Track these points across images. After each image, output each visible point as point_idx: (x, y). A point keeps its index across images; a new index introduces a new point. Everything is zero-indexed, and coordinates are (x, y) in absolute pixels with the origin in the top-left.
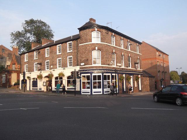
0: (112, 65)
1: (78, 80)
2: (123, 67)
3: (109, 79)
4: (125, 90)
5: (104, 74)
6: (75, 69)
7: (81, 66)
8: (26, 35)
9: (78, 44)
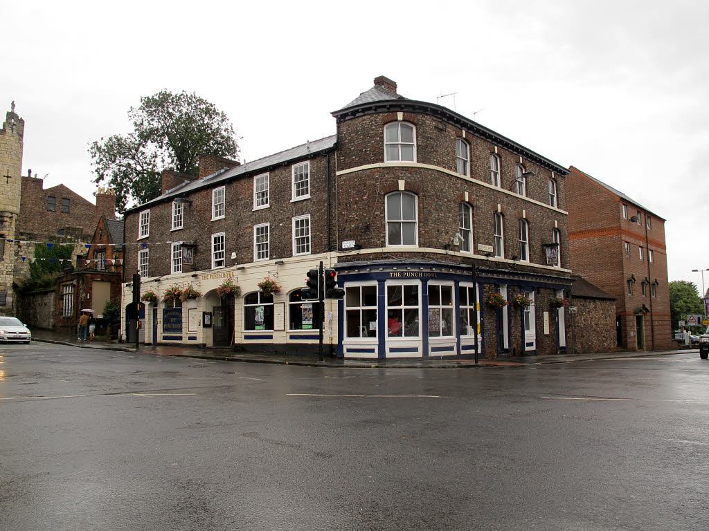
0: (458, 248)
2: (500, 258)
3: (447, 300)
4: (506, 346)
5: (430, 283)
6: (321, 263)
7: (341, 250)
8: (141, 148)
9: (330, 170)
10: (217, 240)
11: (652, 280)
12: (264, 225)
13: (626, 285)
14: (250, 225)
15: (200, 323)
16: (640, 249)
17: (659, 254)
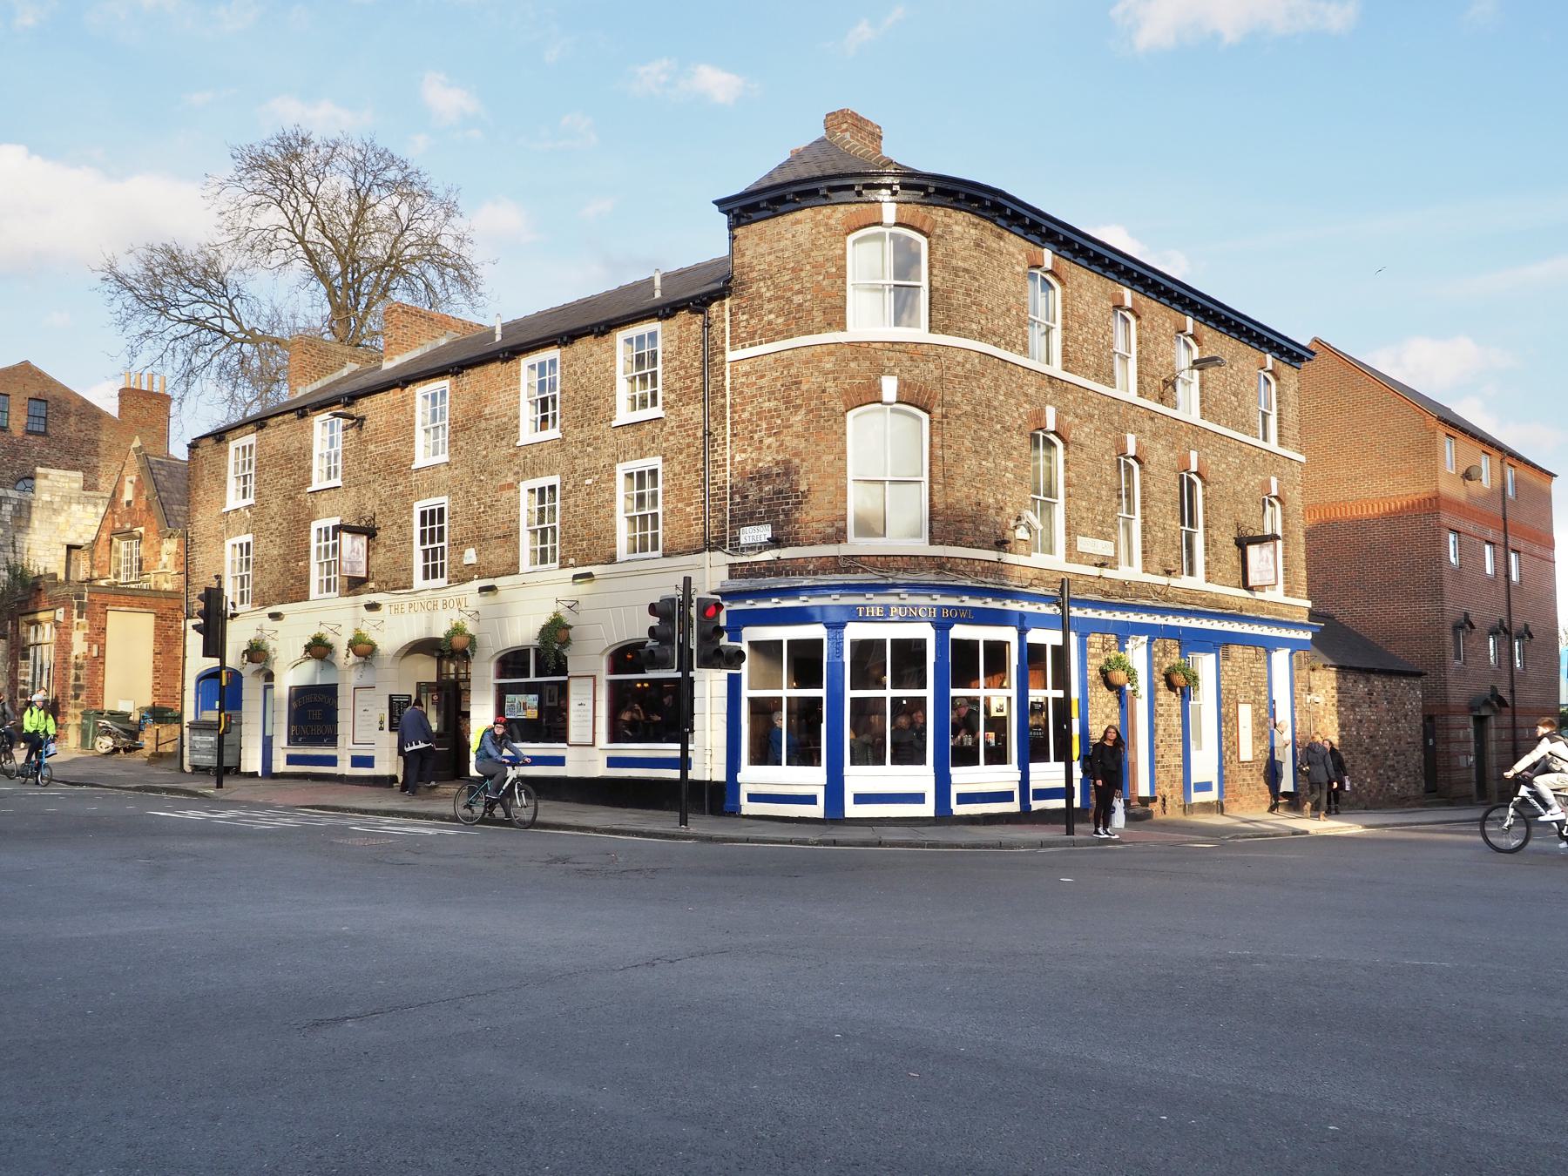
1: (710, 686)
5: (959, 632)
6: (687, 581)
7: (736, 548)
10: (430, 517)
11: (1518, 623)
12: (545, 481)
13: (1449, 639)
14: (510, 480)
15: (381, 722)
16: (1487, 547)
17: (1537, 560)
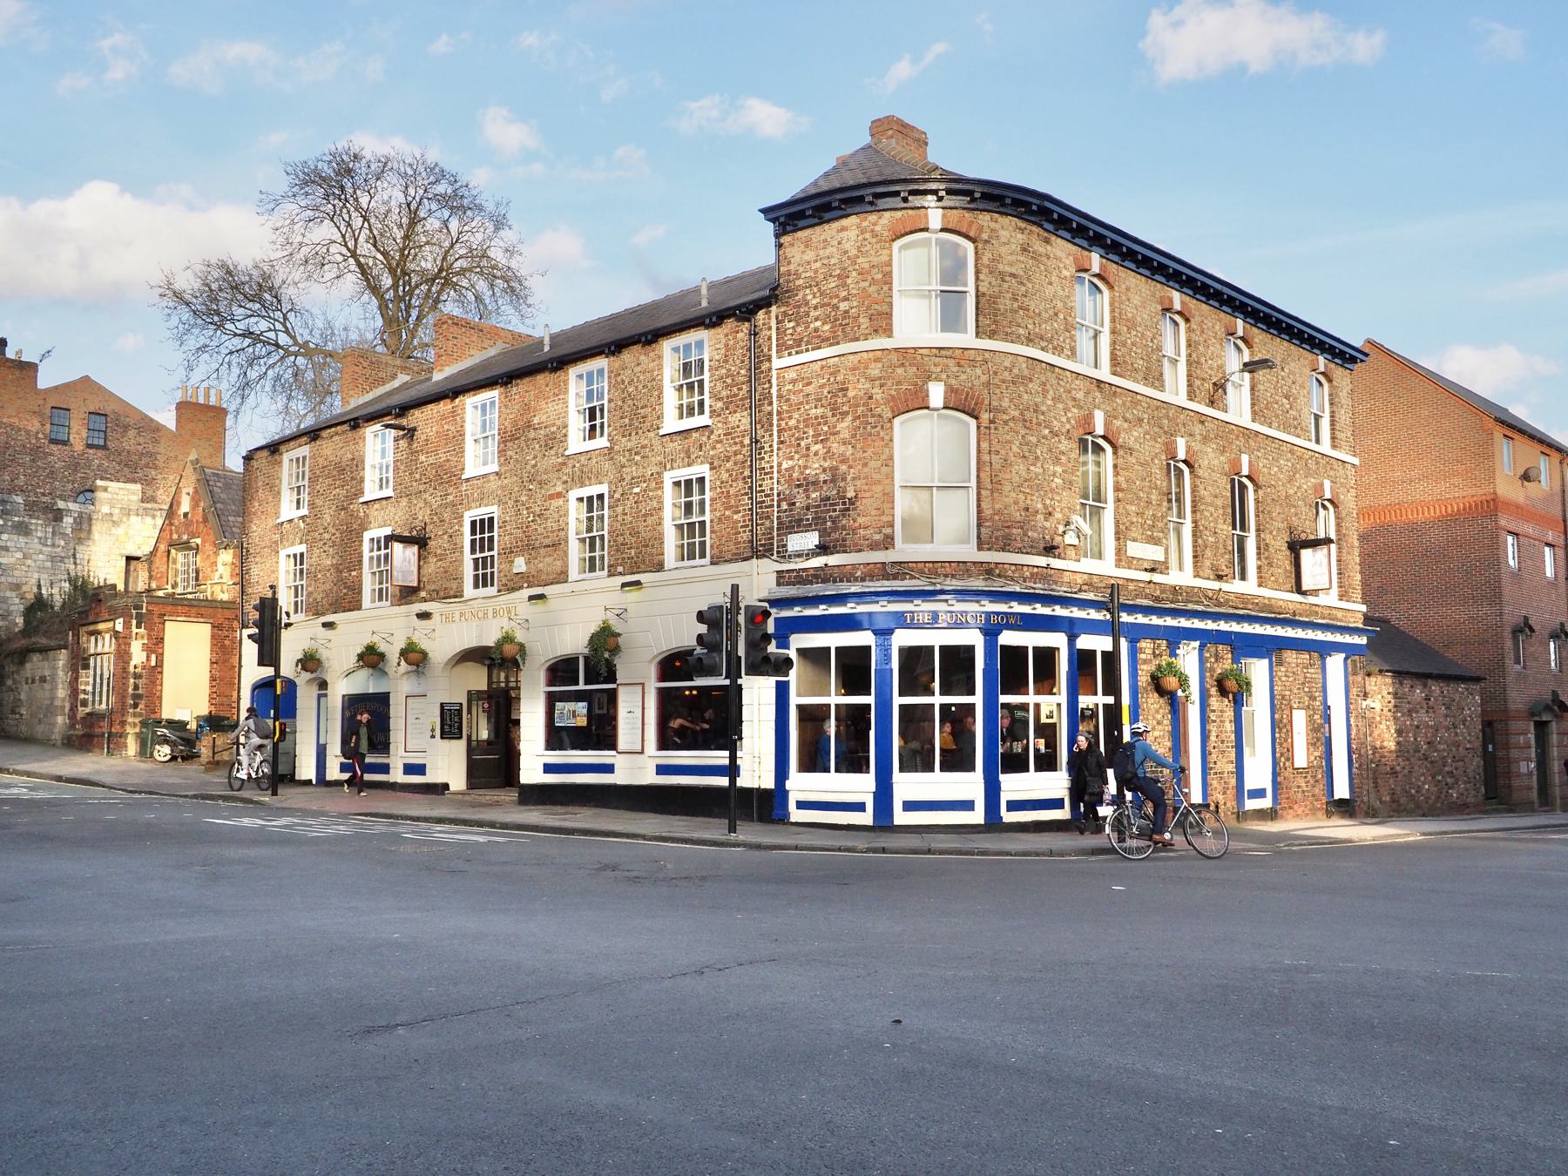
5: (1008, 638)
6: (735, 588)
7: (784, 555)
14: (559, 489)
15: (433, 730)
16: (1547, 549)
